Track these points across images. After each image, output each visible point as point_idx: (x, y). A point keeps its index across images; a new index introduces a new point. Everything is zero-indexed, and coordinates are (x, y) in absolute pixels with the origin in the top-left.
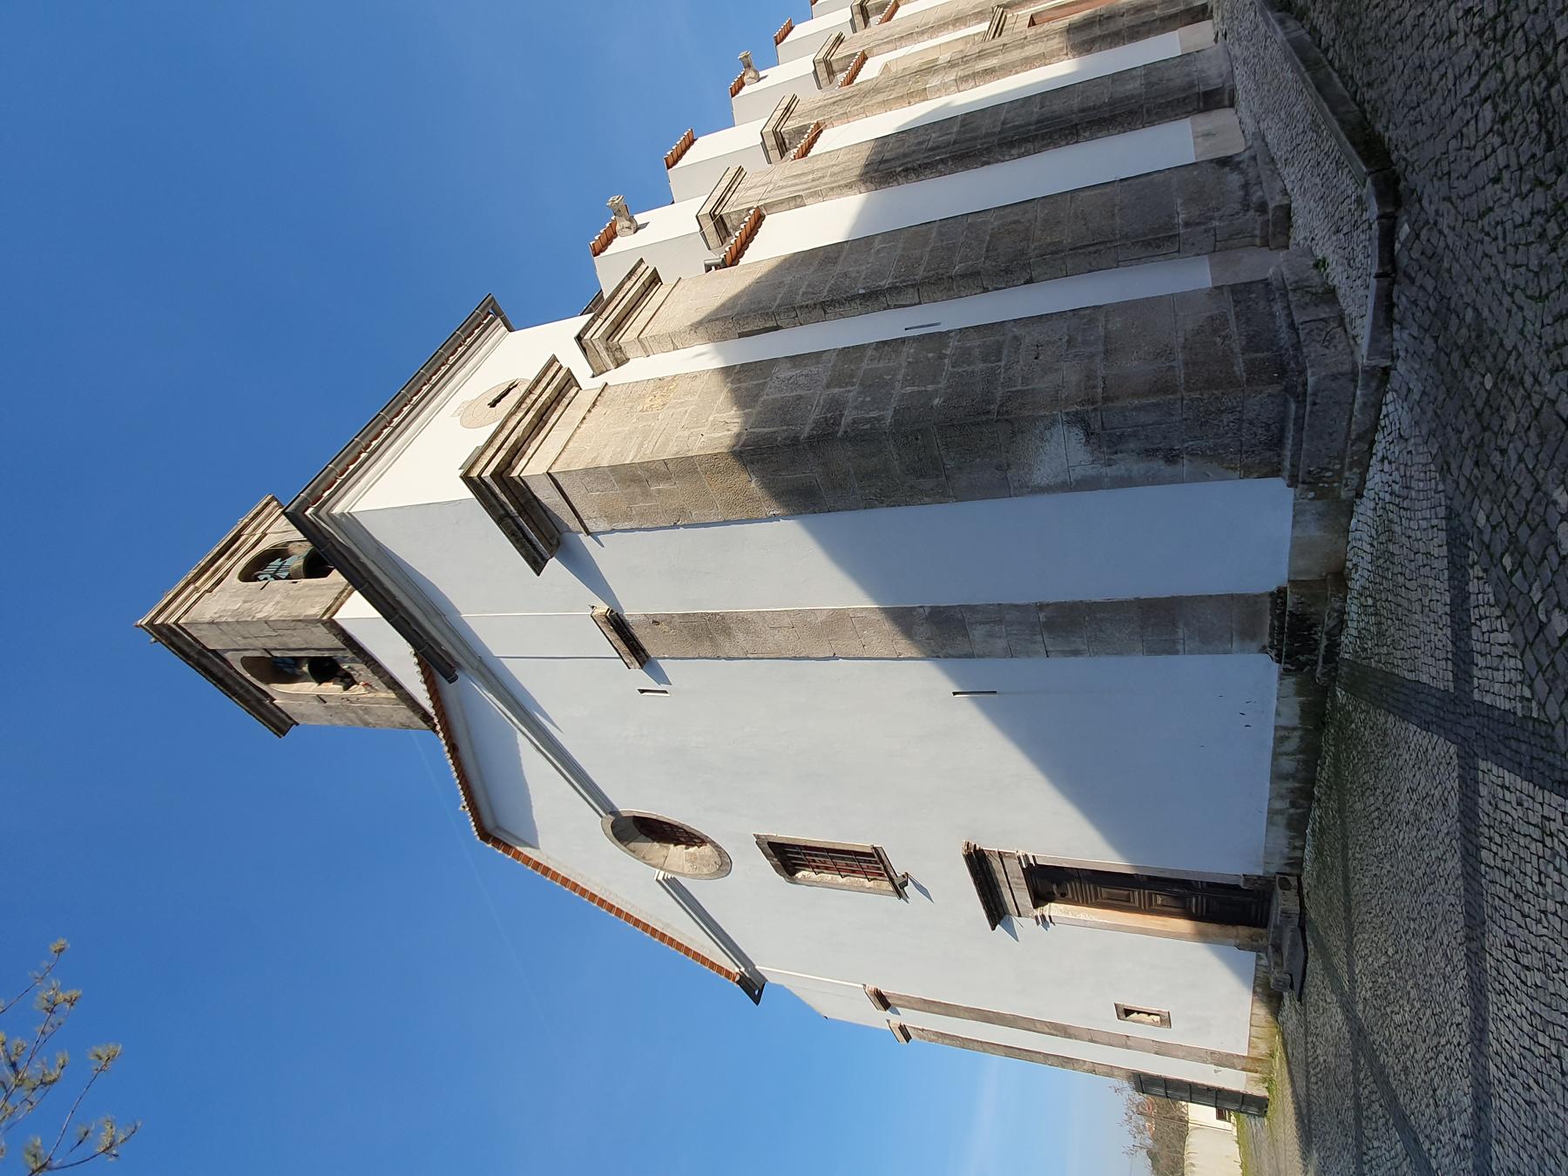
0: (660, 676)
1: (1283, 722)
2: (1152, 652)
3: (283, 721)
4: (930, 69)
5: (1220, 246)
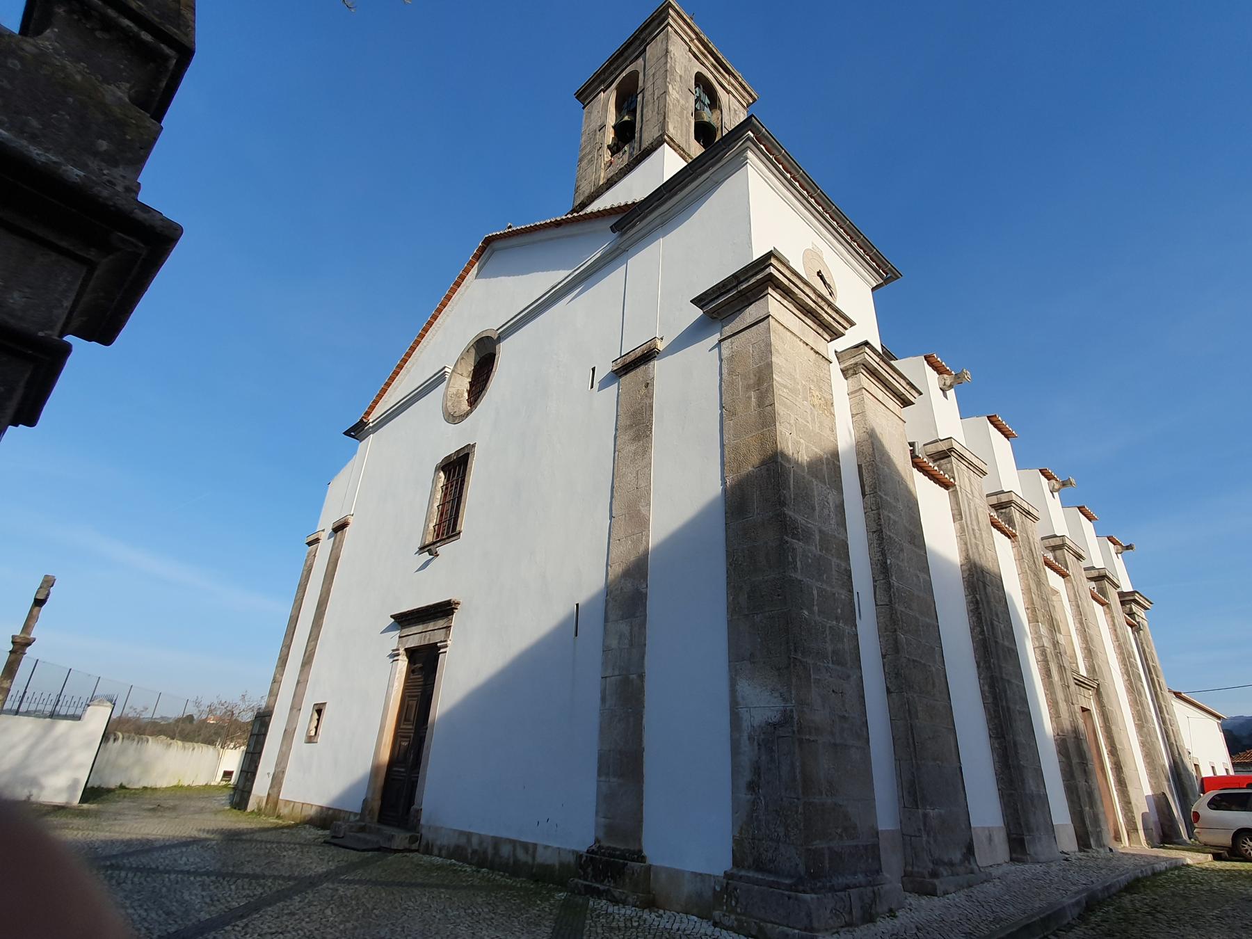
0: (605, 384)
1: (540, 850)
2: (601, 757)
3: (586, 98)
4: (1053, 627)
5: (907, 839)
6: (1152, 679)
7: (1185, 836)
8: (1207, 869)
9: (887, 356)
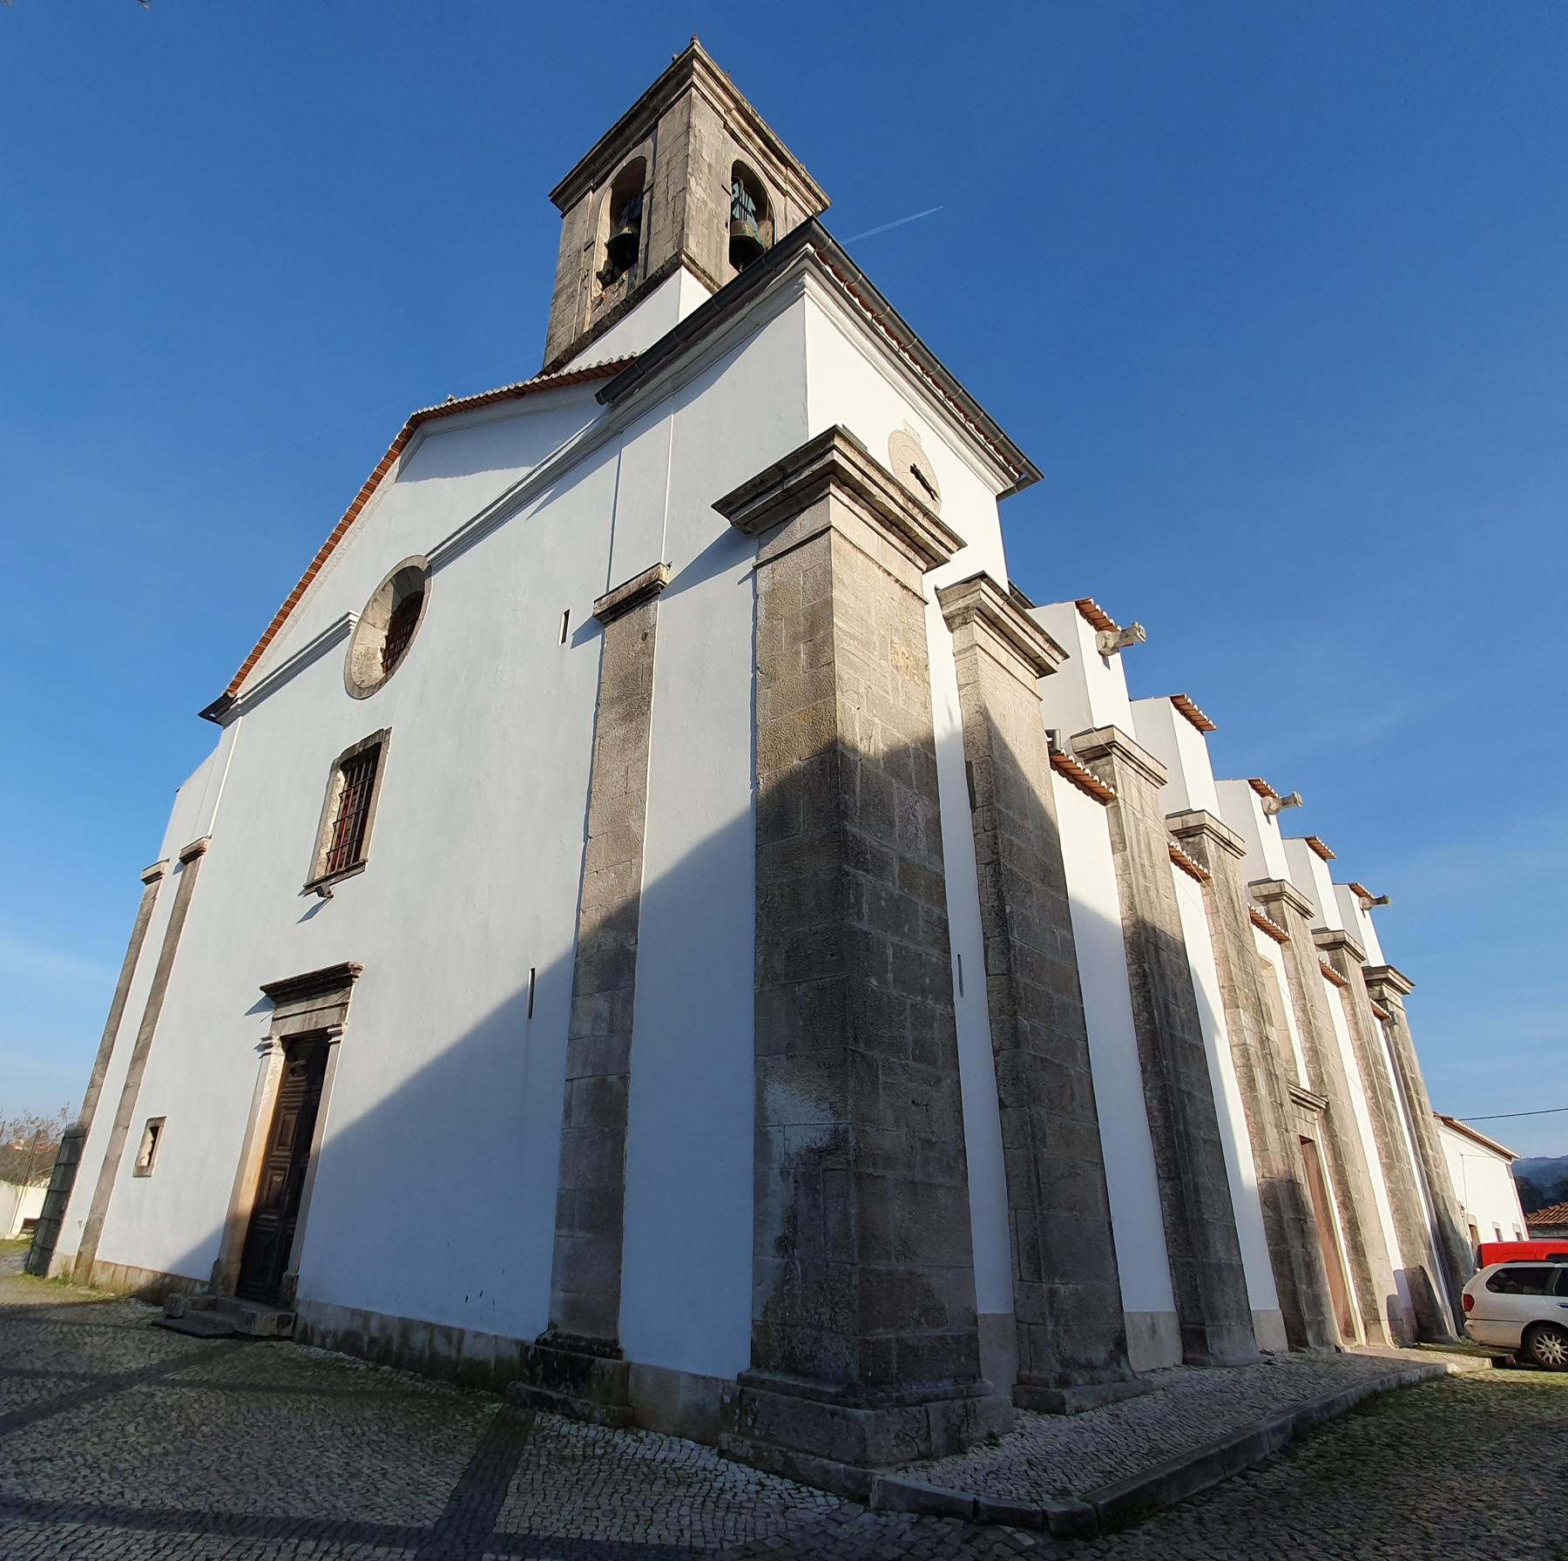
0: (583, 636)
3: (567, 201)
4: (1261, 1014)
5: (1023, 1327)
6: (1410, 1098)
7: (1451, 1330)
8: (1482, 1381)
9: (1019, 600)
